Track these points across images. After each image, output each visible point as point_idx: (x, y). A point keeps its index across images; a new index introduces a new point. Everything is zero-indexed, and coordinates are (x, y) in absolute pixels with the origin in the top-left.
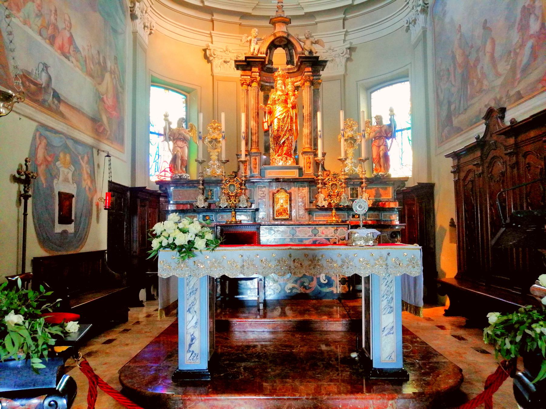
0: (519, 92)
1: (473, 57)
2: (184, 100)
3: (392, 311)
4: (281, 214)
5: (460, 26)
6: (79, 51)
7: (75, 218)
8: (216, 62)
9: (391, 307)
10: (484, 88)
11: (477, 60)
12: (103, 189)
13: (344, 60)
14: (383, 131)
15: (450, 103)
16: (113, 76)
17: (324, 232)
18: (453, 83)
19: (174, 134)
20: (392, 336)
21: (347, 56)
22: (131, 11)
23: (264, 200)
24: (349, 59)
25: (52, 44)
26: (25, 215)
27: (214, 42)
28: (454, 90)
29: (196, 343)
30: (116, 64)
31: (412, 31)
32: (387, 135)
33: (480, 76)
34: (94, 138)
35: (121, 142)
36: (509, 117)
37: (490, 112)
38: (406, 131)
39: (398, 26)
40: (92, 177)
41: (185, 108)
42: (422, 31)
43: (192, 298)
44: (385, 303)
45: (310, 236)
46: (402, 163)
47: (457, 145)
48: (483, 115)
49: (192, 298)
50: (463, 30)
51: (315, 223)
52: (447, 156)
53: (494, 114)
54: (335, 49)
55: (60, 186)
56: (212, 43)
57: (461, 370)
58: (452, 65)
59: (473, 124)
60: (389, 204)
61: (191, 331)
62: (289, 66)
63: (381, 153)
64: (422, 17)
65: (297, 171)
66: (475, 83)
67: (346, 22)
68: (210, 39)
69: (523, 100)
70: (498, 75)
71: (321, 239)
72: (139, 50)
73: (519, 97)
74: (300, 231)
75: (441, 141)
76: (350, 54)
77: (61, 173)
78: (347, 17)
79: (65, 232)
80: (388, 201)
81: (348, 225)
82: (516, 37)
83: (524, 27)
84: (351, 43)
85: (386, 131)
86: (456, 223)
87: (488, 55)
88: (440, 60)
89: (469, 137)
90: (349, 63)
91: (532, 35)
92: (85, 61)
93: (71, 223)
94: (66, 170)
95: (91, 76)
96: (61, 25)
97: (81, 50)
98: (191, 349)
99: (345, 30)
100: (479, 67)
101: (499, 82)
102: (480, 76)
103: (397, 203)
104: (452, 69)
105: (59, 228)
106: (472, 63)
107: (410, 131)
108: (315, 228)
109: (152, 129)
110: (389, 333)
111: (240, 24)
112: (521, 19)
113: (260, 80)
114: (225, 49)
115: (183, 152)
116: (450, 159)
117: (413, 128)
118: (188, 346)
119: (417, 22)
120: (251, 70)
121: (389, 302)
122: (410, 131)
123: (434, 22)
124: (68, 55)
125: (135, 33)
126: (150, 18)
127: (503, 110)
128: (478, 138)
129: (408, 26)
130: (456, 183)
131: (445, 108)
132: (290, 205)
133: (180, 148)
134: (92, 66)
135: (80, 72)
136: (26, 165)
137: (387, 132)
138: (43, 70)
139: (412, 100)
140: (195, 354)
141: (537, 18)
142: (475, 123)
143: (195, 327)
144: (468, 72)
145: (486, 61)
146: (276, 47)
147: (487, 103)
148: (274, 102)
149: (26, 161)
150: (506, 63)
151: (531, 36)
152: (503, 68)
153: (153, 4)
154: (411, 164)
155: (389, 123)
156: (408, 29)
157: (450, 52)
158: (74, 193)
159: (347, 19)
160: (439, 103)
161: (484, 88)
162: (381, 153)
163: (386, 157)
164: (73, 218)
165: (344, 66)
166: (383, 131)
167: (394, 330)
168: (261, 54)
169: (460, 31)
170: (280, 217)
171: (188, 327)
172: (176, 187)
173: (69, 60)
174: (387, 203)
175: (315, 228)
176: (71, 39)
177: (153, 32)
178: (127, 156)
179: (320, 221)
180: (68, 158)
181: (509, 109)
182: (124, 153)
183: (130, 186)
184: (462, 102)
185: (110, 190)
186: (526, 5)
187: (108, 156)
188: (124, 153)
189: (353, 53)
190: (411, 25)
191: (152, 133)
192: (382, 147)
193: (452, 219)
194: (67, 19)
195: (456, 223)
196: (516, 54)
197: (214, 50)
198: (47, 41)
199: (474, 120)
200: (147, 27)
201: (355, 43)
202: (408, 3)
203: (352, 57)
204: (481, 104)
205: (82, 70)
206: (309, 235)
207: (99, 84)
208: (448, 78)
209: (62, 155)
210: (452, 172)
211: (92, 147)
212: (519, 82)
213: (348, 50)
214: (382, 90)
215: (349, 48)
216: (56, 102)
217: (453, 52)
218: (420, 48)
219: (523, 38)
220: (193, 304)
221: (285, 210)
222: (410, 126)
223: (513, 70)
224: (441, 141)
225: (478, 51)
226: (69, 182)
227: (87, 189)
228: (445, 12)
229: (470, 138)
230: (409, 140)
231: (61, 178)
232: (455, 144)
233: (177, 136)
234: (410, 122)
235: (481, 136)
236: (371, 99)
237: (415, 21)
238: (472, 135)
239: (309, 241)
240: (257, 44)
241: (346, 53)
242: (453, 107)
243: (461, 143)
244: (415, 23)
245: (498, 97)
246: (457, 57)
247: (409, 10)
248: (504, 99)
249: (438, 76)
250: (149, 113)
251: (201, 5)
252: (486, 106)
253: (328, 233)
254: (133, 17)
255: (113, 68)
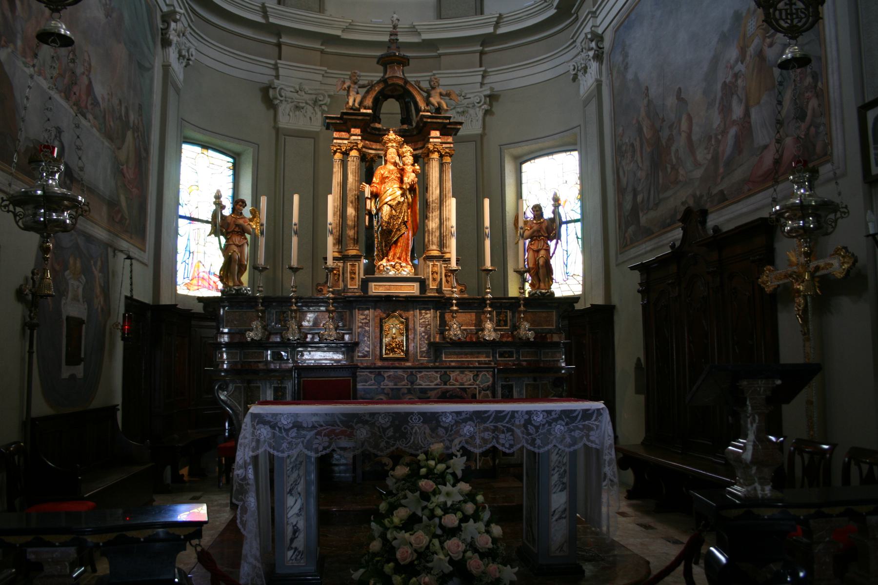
0: (722, 192)
1: (665, 134)
2: (231, 165)
3: (565, 488)
4: (392, 350)
5: (647, 89)
6: (98, 103)
7: (85, 354)
8: (284, 109)
9: (563, 483)
10: (681, 178)
11: (671, 139)
12: (120, 309)
13: (481, 114)
14: (544, 228)
15: (635, 194)
16: (136, 135)
17: (459, 378)
18: (640, 165)
19: (229, 224)
20: (564, 521)
21: (485, 107)
22: (162, 34)
23: (367, 328)
24: (487, 113)
25: (67, 98)
26: (31, 353)
27: (281, 77)
28: (641, 174)
29: (301, 537)
30: (141, 115)
31: (581, 82)
32: (549, 234)
33: (674, 160)
34: (109, 231)
35: (141, 233)
36: (713, 221)
37: (688, 212)
38: (573, 224)
39: (561, 70)
40: (106, 291)
41: (231, 177)
42: (595, 84)
43: (295, 475)
44: (555, 478)
45: (437, 385)
46: (569, 273)
47: (646, 253)
48: (679, 217)
49: (295, 475)
50: (653, 92)
51: (444, 365)
52: (632, 268)
53: (692, 217)
54: (468, 96)
55: (73, 309)
56: (277, 77)
57: (648, 563)
58: (638, 139)
59: (666, 226)
60: (552, 337)
61: (294, 521)
62: (405, 127)
63: (541, 262)
64: (594, 66)
65: (416, 285)
66: (669, 170)
67: (484, 57)
68: (274, 73)
69: (727, 203)
70: (697, 165)
71: (455, 389)
72: (171, 92)
73: (723, 199)
74: (422, 377)
75: (625, 245)
76: (491, 105)
77: (70, 288)
78: (486, 49)
79: (73, 377)
80: (551, 332)
81: (494, 368)
82: (717, 120)
83: (725, 110)
84: (492, 89)
85: (547, 228)
86: (643, 365)
87: (684, 135)
88: (621, 129)
89: (661, 243)
90: (488, 118)
91: (734, 121)
92: (104, 117)
93: (78, 364)
94: (76, 283)
95: (110, 138)
96: (80, 70)
97: (100, 100)
98: (294, 545)
99: (483, 69)
100: (673, 149)
101: (698, 173)
102: (674, 160)
103: (563, 336)
104: (637, 144)
105: (66, 372)
106: (664, 142)
107: (579, 224)
108: (445, 372)
109: (182, 211)
110: (560, 518)
111: (322, 52)
112: (722, 98)
113: (364, 147)
114: (297, 88)
115: (242, 252)
116: (637, 273)
117: (583, 220)
118: (289, 542)
119: (589, 70)
120: (348, 131)
121: (562, 476)
122: (579, 224)
123: (611, 74)
124: (85, 111)
125: (166, 67)
126: (188, 44)
127: (704, 213)
128: (673, 247)
129: (576, 75)
130: (644, 307)
131: (629, 198)
132: (407, 337)
133: (237, 246)
134: (112, 124)
135: (98, 134)
136: (32, 278)
137: (546, 230)
138: (56, 136)
139: (582, 178)
140: (299, 552)
141: (740, 101)
142: (669, 225)
143: (298, 515)
144: (659, 155)
145: (681, 142)
146: (386, 97)
147: (684, 200)
148: (383, 180)
149: (33, 273)
150: (705, 151)
151: (734, 122)
152: (703, 155)
153: (192, 21)
154: (581, 274)
155: (552, 216)
156: (575, 78)
157: (634, 122)
158: (85, 318)
159: (486, 53)
160: (621, 191)
161: (681, 178)
162: (541, 262)
163: (549, 271)
164: (83, 356)
165: (480, 122)
166: (544, 228)
167: (567, 513)
168: (365, 108)
169: (647, 95)
170: (391, 355)
171: (289, 515)
172: (231, 307)
173: (86, 118)
174: (548, 336)
175: (445, 372)
176: (90, 87)
177: (191, 63)
178: (148, 256)
179: (452, 361)
180: (78, 264)
181: (712, 212)
182: (144, 251)
183: (151, 303)
184: (652, 192)
185: (127, 310)
186: (728, 81)
187: (129, 258)
188: (144, 251)
189: (494, 104)
190: (580, 74)
191: (182, 217)
192: (542, 253)
193: (639, 360)
194: (87, 59)
195: (643, 365)
196: (718, 142)
197: (281, 89)
198: (63, 94)
199: (668, 221)
200: (184, 57)
201: (498, 88)
202: (575, 42)
203: (493, 109)
204: (678, 199)
205: (99, 130)
206: (435, 382)
207: (119, 148)
208: (633, 157)
209: (71, 261)
210: (639, 291)
211: (108, 245)
212: (723, 178)
213: (488, 99)
214: (537, 161)
215: (490, 96)
216: (68, 182)
217: (638, 122)
218: (593, 107)
219: (725, 124)
220: (296, 483)
221: (399, 346)
222: (579, 217)
223: (715, 159)
224: (625, 245)
225: (671, 127)
226: (78, 301)
227: (99, 310)
228: (627, 64)
229: (663, 246)
230: (578, 238)
231: (70, 295)
232: (643, 251)
233: (232, 227)
234: (579, 211)
235: (678, 244)
236: (521, 172)
237: (585, 69)
238: (665, 242)
239: (436, 392)
240: (358, 93)
241: (485, 103)
242: (639, 198)
243: (651, 250)
244: (585, 72)
245: (698, 193)
246: (645, 129)
247: (574, 52)
248: (705, 198)
249: (619, 151)
250: (179, 184)
251: (263, 21)
252: (683, 203)
253: (465, 379)
254: (166, 43)
255: (136, 122)
